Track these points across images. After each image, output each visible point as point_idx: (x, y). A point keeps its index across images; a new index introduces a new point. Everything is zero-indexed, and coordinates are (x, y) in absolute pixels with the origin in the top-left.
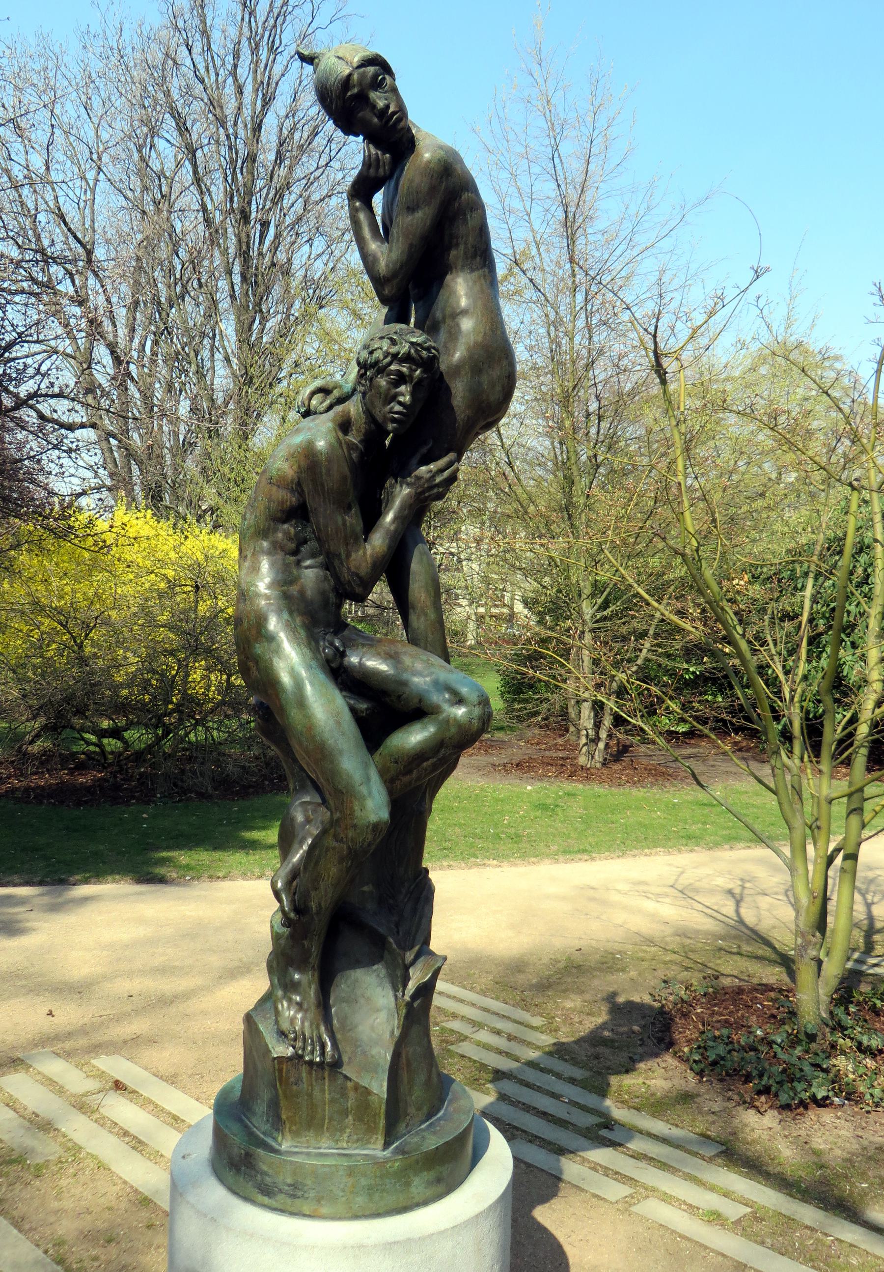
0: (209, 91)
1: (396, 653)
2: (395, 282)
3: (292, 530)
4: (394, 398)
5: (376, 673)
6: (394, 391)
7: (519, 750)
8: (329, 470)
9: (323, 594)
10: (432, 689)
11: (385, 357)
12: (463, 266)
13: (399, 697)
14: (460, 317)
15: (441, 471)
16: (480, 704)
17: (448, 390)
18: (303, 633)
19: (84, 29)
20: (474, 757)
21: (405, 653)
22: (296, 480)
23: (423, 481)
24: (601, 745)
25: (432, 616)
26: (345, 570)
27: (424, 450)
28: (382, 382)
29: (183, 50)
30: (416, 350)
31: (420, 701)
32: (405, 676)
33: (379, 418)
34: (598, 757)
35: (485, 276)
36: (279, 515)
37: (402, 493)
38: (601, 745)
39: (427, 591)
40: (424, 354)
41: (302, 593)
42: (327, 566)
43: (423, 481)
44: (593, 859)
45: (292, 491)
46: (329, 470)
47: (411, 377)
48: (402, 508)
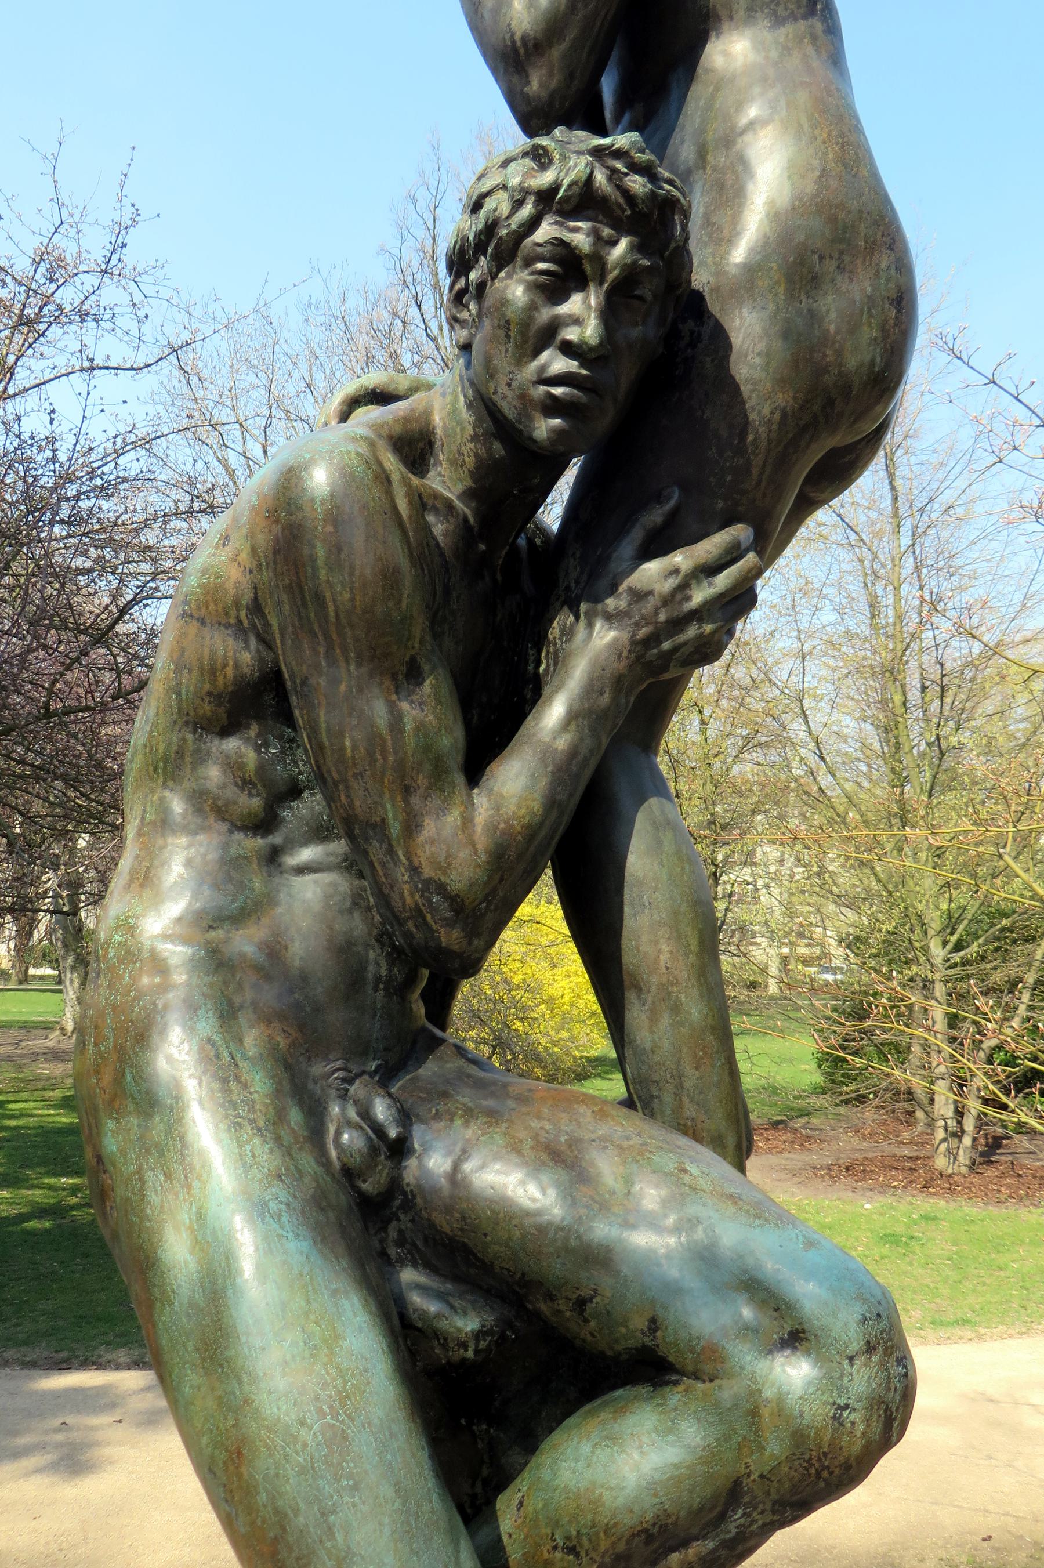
0: (443, 350)
1: (574, 1143)
2: (556, 53)
3: (251, 757)
4: (548, 335)
5: (504, 1213)
6: (546, 314)
7: (847, 1145)
8: (337, 549)
9: (344, 951)
10: (691, 1281)
11: (518, 204)
12: (751, 10)
13: (581, 1304)
14: (748, 138)
15: (709, 570)
16: (870, 1348)
17: (719, 340)
18: (259, 1083)
19: (306, 301)
20: (786, 1155)
21: (604, 1142)
22: (247, 597)
23: (652, 602)
24: (967, 1141)
25: (695, 1010)
26: (402, 875)
27: (656, 516)
28: (515, 289)
29: (414, 311)
30: (613, 175)
31: (654, 1325)
32: (602, 1230)
33: (508, 408)
34: (963, 1158)
35: (814, 38)
36: (207, 708)
37: (589, 648)
38: (967, 1141)
39: (679, 937)
40: (637, 184)
41: (274, 951)
42: (355, 864)
43: (652, 602)
44: (980, 1337)
45: (240, 630)
46: (337, 549)
47: (598, 259)
48: (591, 689)
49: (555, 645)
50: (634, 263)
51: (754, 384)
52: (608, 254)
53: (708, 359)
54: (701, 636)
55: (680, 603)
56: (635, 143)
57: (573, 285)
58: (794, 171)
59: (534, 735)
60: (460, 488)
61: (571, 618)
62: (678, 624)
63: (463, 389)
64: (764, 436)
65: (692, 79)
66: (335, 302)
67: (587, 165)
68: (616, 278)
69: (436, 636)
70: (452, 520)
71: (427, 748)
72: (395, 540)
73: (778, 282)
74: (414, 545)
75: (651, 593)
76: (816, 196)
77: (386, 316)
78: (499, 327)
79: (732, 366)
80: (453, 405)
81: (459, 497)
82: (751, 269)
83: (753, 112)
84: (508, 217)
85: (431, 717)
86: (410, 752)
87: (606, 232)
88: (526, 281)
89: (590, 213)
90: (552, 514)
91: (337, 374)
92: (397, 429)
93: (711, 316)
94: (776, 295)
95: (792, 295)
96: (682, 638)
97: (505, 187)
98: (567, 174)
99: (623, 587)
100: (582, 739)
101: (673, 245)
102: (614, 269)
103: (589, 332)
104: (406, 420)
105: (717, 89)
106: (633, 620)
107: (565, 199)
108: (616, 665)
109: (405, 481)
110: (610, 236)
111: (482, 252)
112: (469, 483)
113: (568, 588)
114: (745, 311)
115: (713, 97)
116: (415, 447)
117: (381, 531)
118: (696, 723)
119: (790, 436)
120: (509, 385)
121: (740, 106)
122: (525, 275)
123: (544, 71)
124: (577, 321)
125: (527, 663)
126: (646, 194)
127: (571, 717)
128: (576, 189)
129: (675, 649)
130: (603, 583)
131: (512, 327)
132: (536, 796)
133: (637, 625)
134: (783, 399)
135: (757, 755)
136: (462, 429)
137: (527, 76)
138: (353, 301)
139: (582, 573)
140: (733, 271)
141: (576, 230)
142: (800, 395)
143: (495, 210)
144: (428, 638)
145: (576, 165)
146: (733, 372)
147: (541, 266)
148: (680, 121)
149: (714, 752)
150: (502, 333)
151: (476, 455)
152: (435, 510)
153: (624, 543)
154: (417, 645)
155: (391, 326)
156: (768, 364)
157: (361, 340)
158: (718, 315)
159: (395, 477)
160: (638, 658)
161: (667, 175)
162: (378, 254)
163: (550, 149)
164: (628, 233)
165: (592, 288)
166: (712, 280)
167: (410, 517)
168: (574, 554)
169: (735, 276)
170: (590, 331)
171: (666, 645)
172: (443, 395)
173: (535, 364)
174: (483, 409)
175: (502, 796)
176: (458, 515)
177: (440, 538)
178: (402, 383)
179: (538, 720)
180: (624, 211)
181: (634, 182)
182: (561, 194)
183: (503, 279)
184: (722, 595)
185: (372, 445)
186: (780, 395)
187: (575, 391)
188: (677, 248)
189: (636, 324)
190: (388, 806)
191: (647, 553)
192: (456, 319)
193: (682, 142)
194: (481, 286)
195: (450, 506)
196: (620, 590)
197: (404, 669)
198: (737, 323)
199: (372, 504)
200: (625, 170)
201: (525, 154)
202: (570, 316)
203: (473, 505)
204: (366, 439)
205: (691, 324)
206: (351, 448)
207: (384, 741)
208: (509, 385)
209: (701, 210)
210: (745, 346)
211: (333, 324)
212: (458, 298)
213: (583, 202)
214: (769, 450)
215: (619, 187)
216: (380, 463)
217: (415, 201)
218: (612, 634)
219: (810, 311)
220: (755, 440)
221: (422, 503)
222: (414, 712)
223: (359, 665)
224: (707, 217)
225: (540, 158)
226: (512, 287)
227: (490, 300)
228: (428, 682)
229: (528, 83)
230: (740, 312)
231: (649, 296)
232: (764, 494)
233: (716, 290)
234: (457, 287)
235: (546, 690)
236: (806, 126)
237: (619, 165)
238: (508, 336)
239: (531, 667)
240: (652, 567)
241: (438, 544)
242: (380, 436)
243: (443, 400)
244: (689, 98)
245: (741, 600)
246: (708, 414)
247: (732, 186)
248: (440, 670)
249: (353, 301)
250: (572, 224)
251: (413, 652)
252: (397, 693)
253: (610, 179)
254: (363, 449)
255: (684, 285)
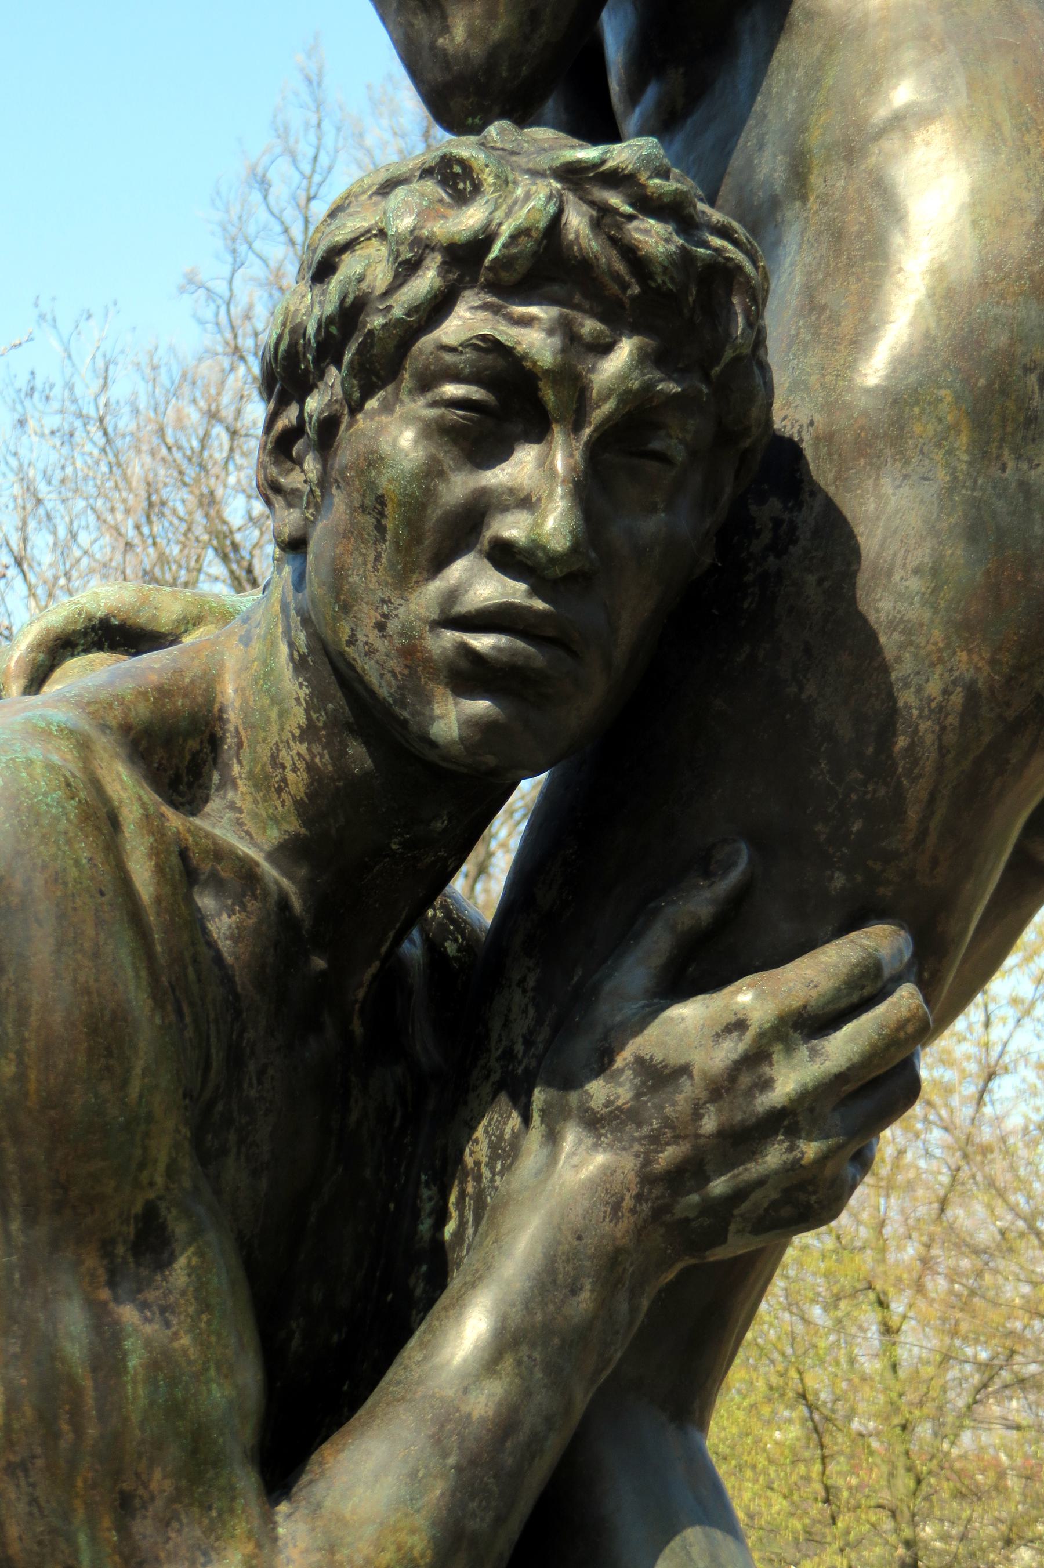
4: (464, 529)
6: (460, 485)
11: (407, 269)
14: (891, 143)
15: (814, 1023)
17: (836, 537)
19: (22, 382)
23: (687, 1091)
27: (698, 904)
28: (398, 435)
30: (603, 218)
33: (379, 673)
37: (548, 1189)
40: (653, 236)
43: (687, 1091)
47: (571, 379)
48: (551, 1280)
49: (478, 1178)
50: (648, 388)
51: (908, 631)
52: (593, 370)
53: (811, 579)
54: (794, 1167)
55: (749, 1094)
56: (648, 160)
57: (519, 428)
58: (979, 208)
59: (420, 1382)
60: (274, 836)
61: (515, 1120)
62: (744, 1139)
63: (287, 632)
64: (929, 739)
65: (781, 28)
66: (87, 388)
67: (550, 197)
68: (608, 418)
69: (206, 1157)
70: (253, 905)
71: (175, 1409)
72: (121, 952)
73: (955, 428)
74: (163, 960)
75: (684, 1070)
76: (1030, 262)
77: (194, 416)
78: (363, 508)
79: (860, 593)
80: (265, 663)
81: (270, 857)
82: (902, 400)
83: (903, 93)
84: (387, 294)
85: (185, 1340)
86: (135, 1418)
87: (589, 326)
88: (419, 418)
89: (556, 289)
90: (482, 886)
91: (84, 538)
92: (142, 711)
93: (816, 490)
94: (950, 452)
95: (983, 453)
96: (753, 1170)
97: (382, 234)
98: (509, 214)
99: (624, 1058)
100: (527, 1394)
101: (729, 354)
102: (606, 399)
103: (553, 525)
104: (163, 692)
105: (830, 49)
106: (645, 1130)
107: (504, 263)
108: (607, 1227)
109: (151, 822)
110: (597, 335)
111: (327, 361)
112: (294, 825)
113: (508, 1055)
114: (887, 485)
115: (820, 65)
116: (178, 749)
117: (90, 931)
118: (874, 1331)
119: (986, 739)
120: (381, 627)
121: (875, 83)
122: (420, 407)
123: (478, 9)
124: (526, 502)
125: (416, 1217)
126: (669, 255)
127: (505, 1343)
128: (526, 244)
129: (738, 1195)
130: (582, 1047)
131: (389, 510)
132: (421, 1521)
133: (655, 1140)
134: (967, 663)
135: (1015, 1406)
136: (281, 714)
137: (444, 17)
138: (126, 385)
139: (539, 1021)
140: (863, 402)
141: (526, 322)
142: (1006, 657)
143: (361, 279)
144: (186, 1163)
145: (528, 196)
146: (862, 607)
147: (451, 390)
148: (757, 107)
149: (911, 1396)
150: (369, 521)
151: (310, 768)
152: (217, 884)
153: (629, 961)
154: (160, 1180)
155: (204, 440)
156: (935, 591)
157: (138, 467)
158: (831, 490)
159: (130, 816)
160: (658, 1213)
161: (716, 216)
162: (182, 290)
163: (475, 165)
164: (634, 330)
165: (558, 435)
166: (818, 419)
167: (158, 900)
168: (522, 981)
169: (865, 413)
170: (553, 524)
171: (719, 1186)
172: (246, 640)
173: (435, 587)
174: (326, 671)
175: (340, 1519)
176: (266, 894)
177: (225, 946)
178: (166, 608)
179: (430, 1348)
180: (625, 286)
181: (646, 232)
182: (495, 252)
183: (374, 413)
184: (840, 1078)
185: (84, 746)
186: (964, 656)
187: (520, 644)
188: (738, 359)
189: (653, 509)
190: (82, 1539)
191: (682, 980)
192: (276, 488)
193: (761, 146)
194: (329, 427)
195: (248, 875)
196: (619, 1062)
197: (131, 1230)
198: (871, 507)
199: (73, 872)
200: (627, 209)
201: (427, 173)
202: (511, 491)
203: (303, 872)
204: (69, 733)
205: (774, 505)
206: (36, 752)
207: (78, 1391)
208: (381, 627)
209: (799, 279)
210: (888, 554)
211: (79, 435)
212: (282, 446)
213: (542, 267)
214: (940, 769)
215: (615, 242)
216: (96, 785)
217: (264, 185)
218: (600, 1159)
219: (1024, 485)
220: (912, 746)
221: (187, 868)
222: (148, 1329)
223: (30, 1220)
224: (809, 292)
225: (455, 179)
226: (393, 429)
227: (345, 455)
228: (182, 1261)
229: (446, 29)
230: (877, 485)
231: (679, 455)
232: (935, 862)
233: (827, 439)
234: (281, 424)
235: (456, 1282)
236: (1007, 126)
237: (615, 200)
238: (381, 528)
239: (425, 1226)
240: (690, 1014)
241: (218, 958)
242: (104, 727)
243: (242, 650)
244: (774, 63)
245: (885, 1087)
246: (811, 690)
247: (860, 235)
248: (211, 1236)
249: (126, 385)
250: (519, 310)
251: (151, 1195)
252: (112, 1284)
253: (596, 225)
254: (63, 756)
255: (755, 432)
